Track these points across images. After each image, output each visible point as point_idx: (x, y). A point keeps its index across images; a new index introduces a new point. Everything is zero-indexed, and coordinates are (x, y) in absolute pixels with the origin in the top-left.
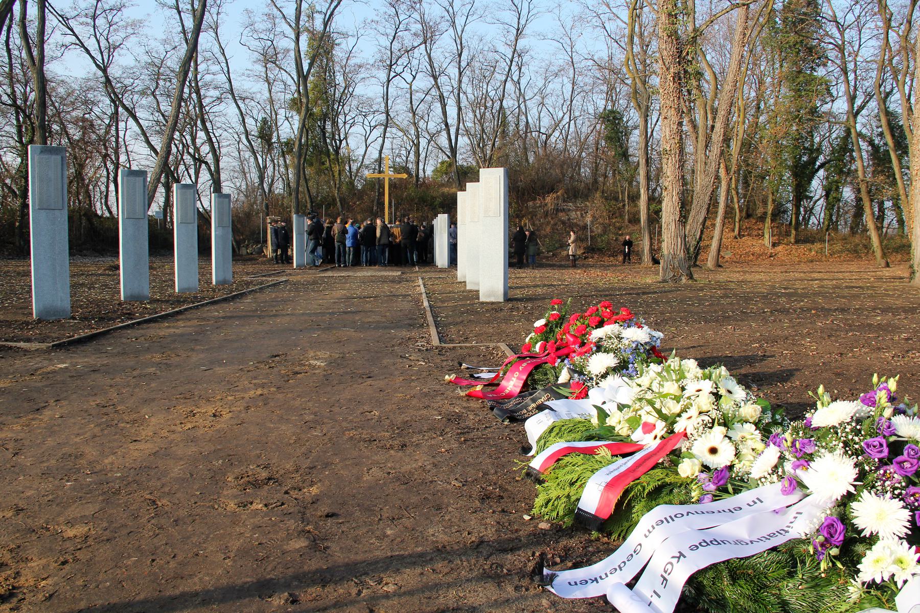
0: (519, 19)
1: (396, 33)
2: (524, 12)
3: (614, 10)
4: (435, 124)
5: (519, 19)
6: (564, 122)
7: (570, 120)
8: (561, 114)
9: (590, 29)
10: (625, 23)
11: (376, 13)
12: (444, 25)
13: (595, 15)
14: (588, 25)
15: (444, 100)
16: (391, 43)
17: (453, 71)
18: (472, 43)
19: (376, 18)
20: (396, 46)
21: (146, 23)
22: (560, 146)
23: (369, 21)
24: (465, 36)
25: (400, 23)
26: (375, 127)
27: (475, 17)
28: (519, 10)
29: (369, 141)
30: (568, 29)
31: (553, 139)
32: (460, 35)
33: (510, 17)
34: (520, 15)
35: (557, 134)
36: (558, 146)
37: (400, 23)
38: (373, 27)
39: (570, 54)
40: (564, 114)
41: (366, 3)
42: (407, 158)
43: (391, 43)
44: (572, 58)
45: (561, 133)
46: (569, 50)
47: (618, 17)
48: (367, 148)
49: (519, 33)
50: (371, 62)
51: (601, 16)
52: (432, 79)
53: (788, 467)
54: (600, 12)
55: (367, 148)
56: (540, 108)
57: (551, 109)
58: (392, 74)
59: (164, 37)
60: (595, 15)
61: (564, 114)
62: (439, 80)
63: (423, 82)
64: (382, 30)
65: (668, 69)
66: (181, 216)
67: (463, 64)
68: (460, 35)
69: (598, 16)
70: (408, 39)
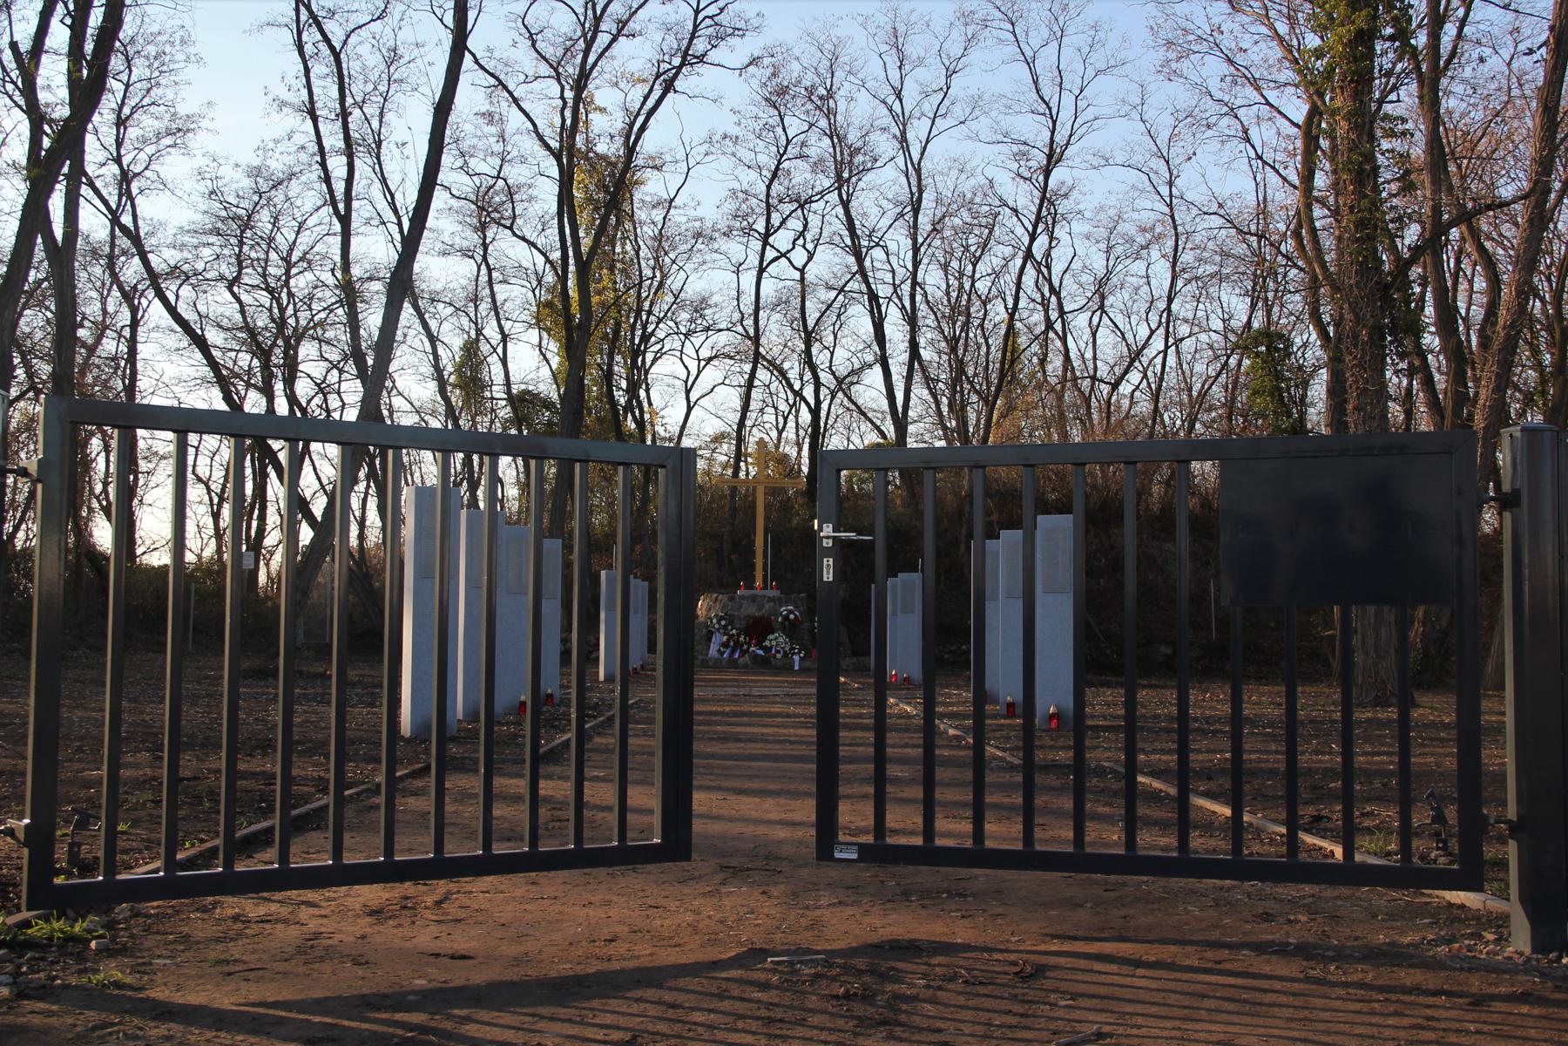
0: (1053, 132)
1: (779, 163)
2: (1065, 116)
3: (1272, 96)
4: (847, 355)
5: (1053, 132)
6: (1149, 352)
7: (1167, 347)
8: (1143, 332)
9: (1214, 145)
10: (1296, 125)
11: (735, 118)
12: (885, 145)
13: (1225, 109)
14: (1210, 133)
15: (879, 306)
16: (769, 187)
17: (899, 240)
18: (942, 182)
19: (734, 131)
20: (777, 188)
21: (205, 123)
22: (1144, 406)
23: (717, 137)
24: (926, 166)
25: (788, 142)
26: (710, 360)
27: (949, 122)
28: (1054, 113)
29: (694, 396)
30: (1162, 140)
31: (1126, 388)
32: (915, 161)
33: (1035, 130)
34: (1054, 123)
35: (1135, 377)
36: (1137, 409)
37: (788, 142)
38: (729, 150)
39: (1168, 200)
40: (1152, 332)
41: (715, 101)
42: (780, 433)
43: (769, 187)
44: (1170, 206)
45: (1145, 376)
46: (1165, 190)
47: (1280, 113)
48: (690, 409)
49: (1053, 158)
50: (722, 226)
51: (1241, 113)
52: (851, 260)
53: (965, 214)
54: (1238, 102)
55: (690, 409)
56: (1095, 320)
57: (1119, 320)
58: (770, 254)
59: (256, 162)
60: (1225, 109)
61: (1152, 332)
62: (868, 261)
63: (830, 263)
64: (747, 156)
65: (1452, 78)
66: (1497, 639)
67: (924, 222)
68: (915, 161)
69: (1233, 112)
70: (800, 175)
